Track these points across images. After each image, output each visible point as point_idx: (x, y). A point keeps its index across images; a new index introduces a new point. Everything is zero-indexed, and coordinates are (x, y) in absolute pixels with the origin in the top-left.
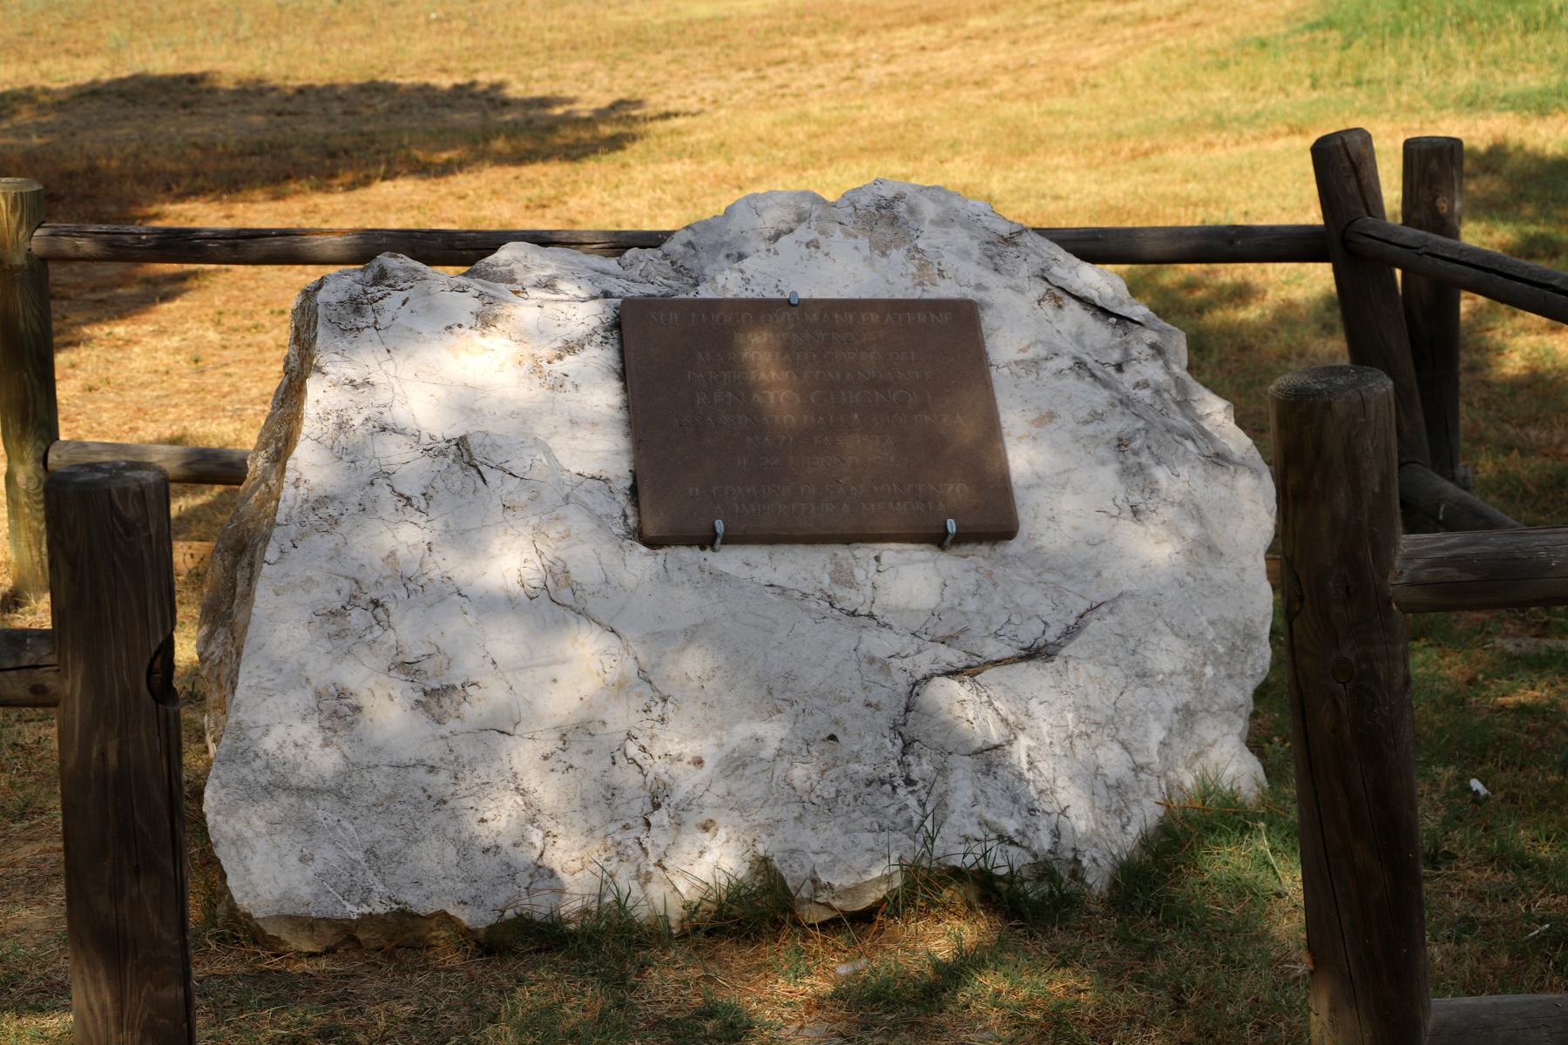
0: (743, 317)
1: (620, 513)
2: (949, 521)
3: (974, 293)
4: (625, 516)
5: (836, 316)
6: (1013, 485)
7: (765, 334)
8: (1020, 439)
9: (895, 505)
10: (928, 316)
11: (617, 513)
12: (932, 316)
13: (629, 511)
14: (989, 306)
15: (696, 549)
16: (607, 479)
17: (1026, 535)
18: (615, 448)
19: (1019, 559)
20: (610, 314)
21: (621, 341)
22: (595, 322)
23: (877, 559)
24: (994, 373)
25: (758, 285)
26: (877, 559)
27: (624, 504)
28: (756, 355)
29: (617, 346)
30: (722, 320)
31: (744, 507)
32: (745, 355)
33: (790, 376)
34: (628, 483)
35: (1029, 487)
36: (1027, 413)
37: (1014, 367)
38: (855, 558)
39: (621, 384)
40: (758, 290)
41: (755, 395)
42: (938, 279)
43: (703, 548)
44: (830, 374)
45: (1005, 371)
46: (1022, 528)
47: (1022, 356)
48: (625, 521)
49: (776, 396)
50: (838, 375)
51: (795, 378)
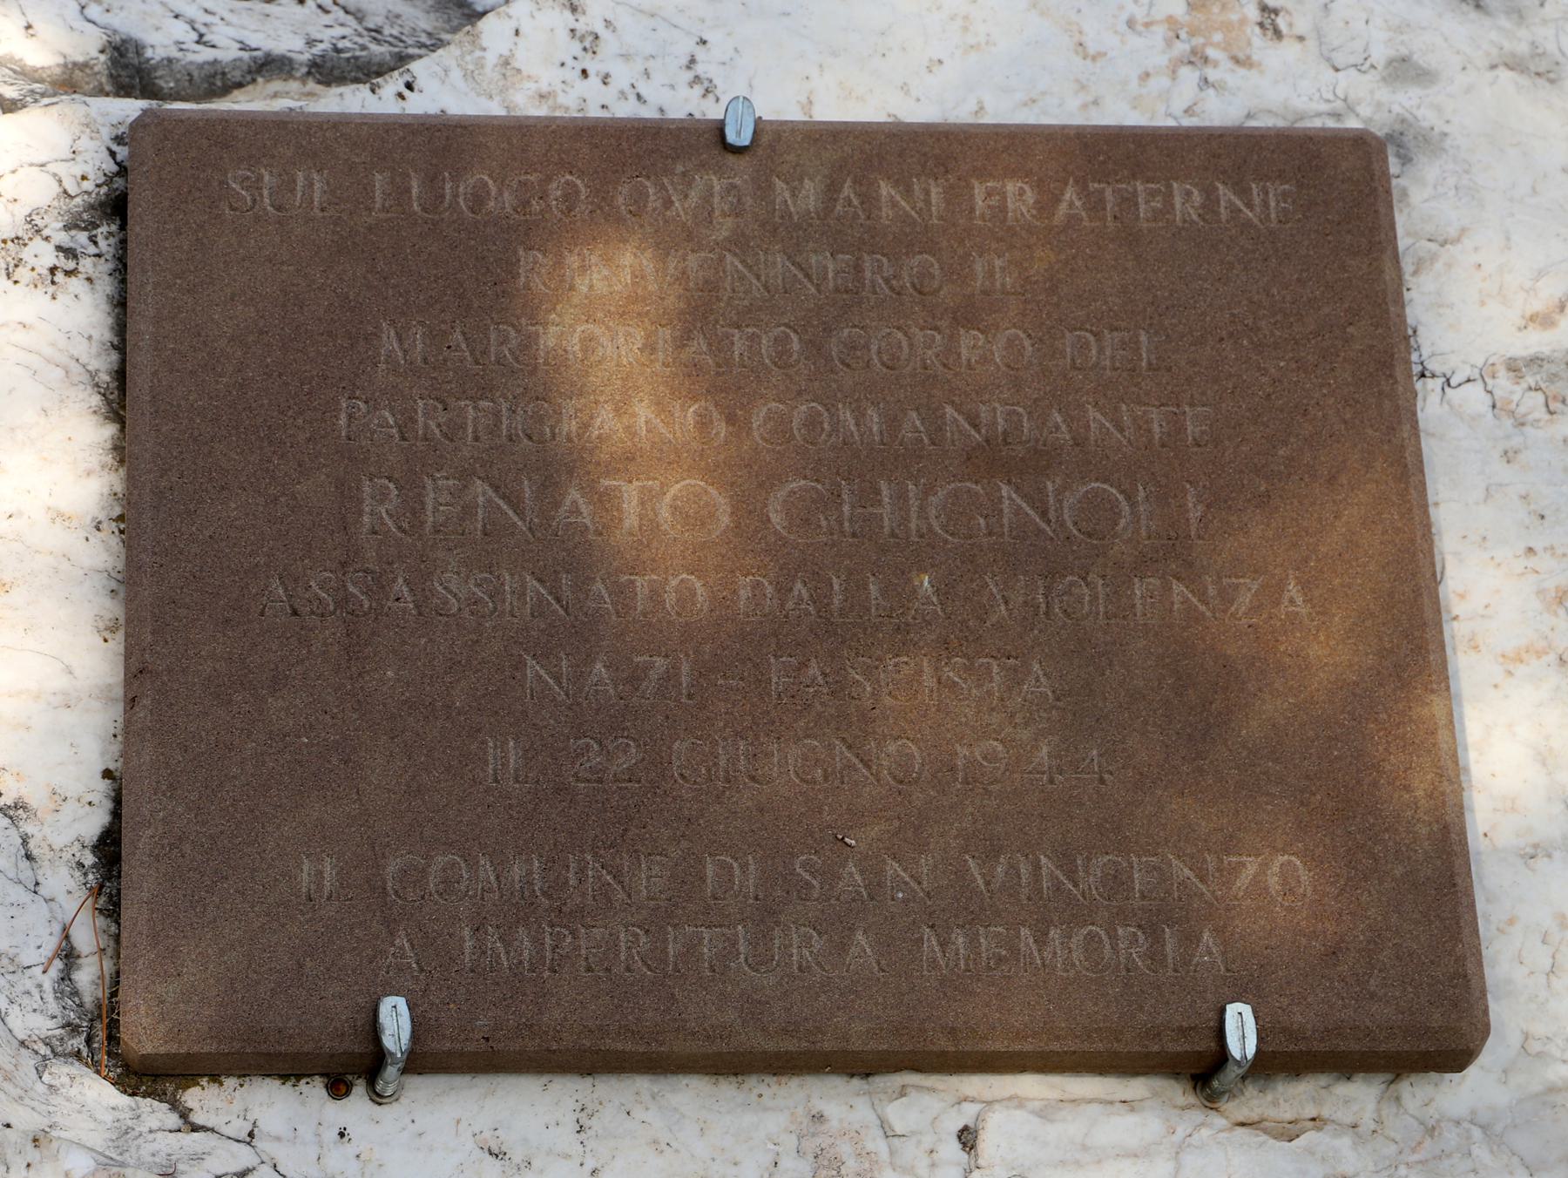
0: (555, 190)
1: (51, 944)
2: (1232, 1010)
3: (1383, 94)
4: (68, 955)
5: (885, 189)
6: (1475, 841)
7: (627, 258)
8: (1513, 659)
9: (1041, 940)
10: (1209, 193)
11: (39, 945)
12: (1225, 193)
13: (85, 938)
14: (1432, 142)
15: (315, 1090)
16: (19, 805)
17: (1515, 1039)
18: (61, 682)
19: (1484, 1128)
20: (94, 163)
21: (121, 269)
22: (38, 192)
23: (967, 1138)
24: (1431, 406)
25: (626, 57)
26: (967, 1138)
27: (69, 905)
28: (588, 342)
29: (106, 286)
30: (478, 199)
31: (493, 941)
32: (549, 339)
33: (703, 423)
34: (94, 823)
35: (1532, 854)
36: (1544, 562)
37: (1503, 384)
38: (888, 1133)
39: (110, 430)
40: (623, 76)
41: (574, 494)
42: (1258, 43)
43: (338, 1088)
44: (847, 416)
45: (1473, 398)
46: (1499, 1011)
47: (1536, 342)
48: (66, 977)
49: (648, 499)
50: (874, 417)
51: (721, 429)
